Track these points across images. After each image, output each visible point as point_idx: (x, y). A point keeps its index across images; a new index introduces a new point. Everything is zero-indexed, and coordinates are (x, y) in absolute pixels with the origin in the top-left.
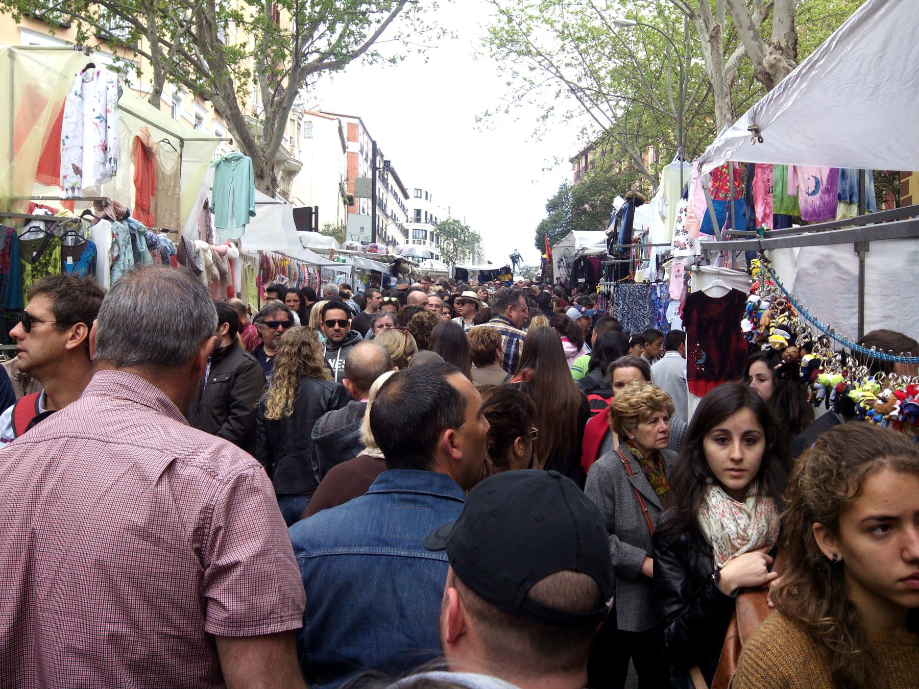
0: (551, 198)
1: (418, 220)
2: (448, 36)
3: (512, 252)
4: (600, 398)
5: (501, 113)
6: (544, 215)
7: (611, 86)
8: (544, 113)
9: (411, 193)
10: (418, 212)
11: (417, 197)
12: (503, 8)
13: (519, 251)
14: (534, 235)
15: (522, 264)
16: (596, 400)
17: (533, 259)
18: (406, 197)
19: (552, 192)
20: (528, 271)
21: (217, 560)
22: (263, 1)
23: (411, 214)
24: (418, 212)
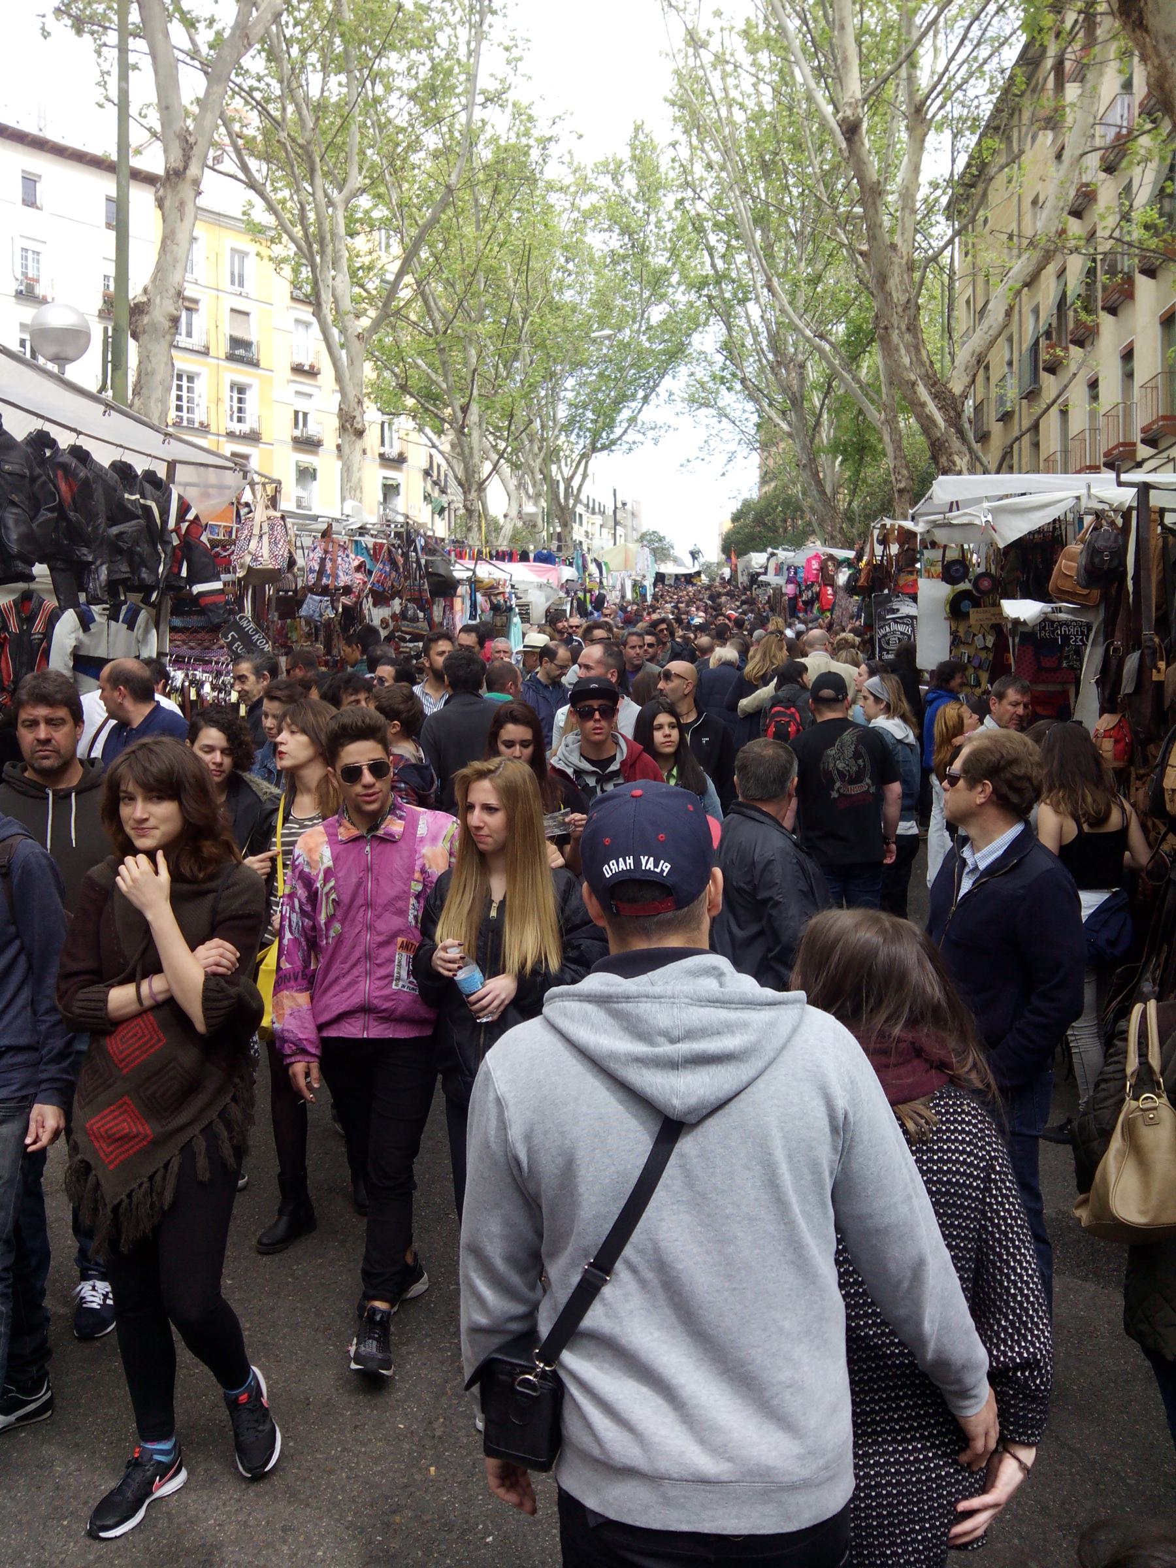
3: (692, 548)
6: (728, 525)
17: (712, 553)
19: (735, 506)
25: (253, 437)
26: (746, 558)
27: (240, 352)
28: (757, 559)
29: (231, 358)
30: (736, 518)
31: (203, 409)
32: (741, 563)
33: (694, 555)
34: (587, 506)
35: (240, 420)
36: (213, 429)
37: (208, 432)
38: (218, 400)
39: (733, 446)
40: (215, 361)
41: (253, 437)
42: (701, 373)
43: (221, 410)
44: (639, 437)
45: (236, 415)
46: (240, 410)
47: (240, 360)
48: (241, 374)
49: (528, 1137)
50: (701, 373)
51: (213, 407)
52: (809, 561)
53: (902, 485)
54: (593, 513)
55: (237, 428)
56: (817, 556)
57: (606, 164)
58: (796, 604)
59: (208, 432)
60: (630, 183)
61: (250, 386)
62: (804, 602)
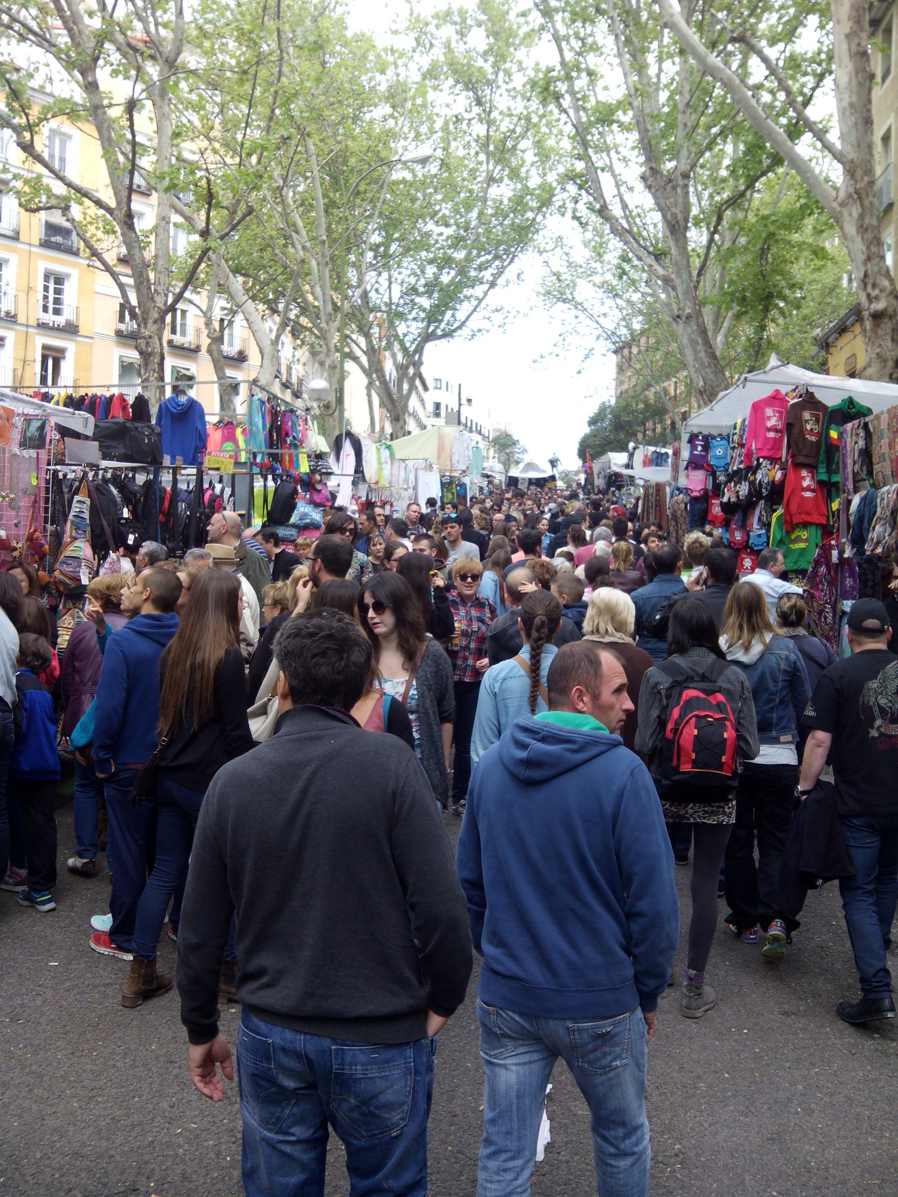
0: (592, 415)
1: (437, 415)
2: (521, 315)
3: (551, 457)
4: (702, 695)
5: (553, 356)
6: (585, 430)
7: (513, 223)
8: (586, 352)
9: (430, 383)
10: (438, 406)
11: (436, 388)
12: (555, 270)
13: (558, 456)
14: (577, 446)
15: (561, 467)
16: (698, 698)
17: (572, 463)
18: (426, 388)
19: (593, 409)
20: (567, 475)
21: (54, 644)
22: (3, 570)
23: (430, 408)
24: (438, 406)
25: (71, 329)
26: (603, 459)
27: (58, 239)
28: (617, 460)
29: (46, 244)
30: (593, 422)
31: (11, 297)
32: (596, 466)
33: (553, 463)
34: (466, 425)
35: (57, 312)
36: (21, 319)
37: (15, 322)
38: (30, 289)
39: (591, 342)
40: (27, 247)
41: (71, 329)
42: (557, 263)
43: (32, 300)
44: (485, 324)
45: (51, 306)
46: (57, 301)
47: (57, 247)
48: (58, 263)
49: (482, 781)
50: (557, 263)
51: (22, 297)
52: (758, 408)
53: (880, 306)
54: (471, 431)
55: (50, 318)
56: (776, 399)
57: (448, 14)
58: (706, 511)
59: (15, 322)
60: (478, 39)
61: (68, 276)
62: (727, 508)
